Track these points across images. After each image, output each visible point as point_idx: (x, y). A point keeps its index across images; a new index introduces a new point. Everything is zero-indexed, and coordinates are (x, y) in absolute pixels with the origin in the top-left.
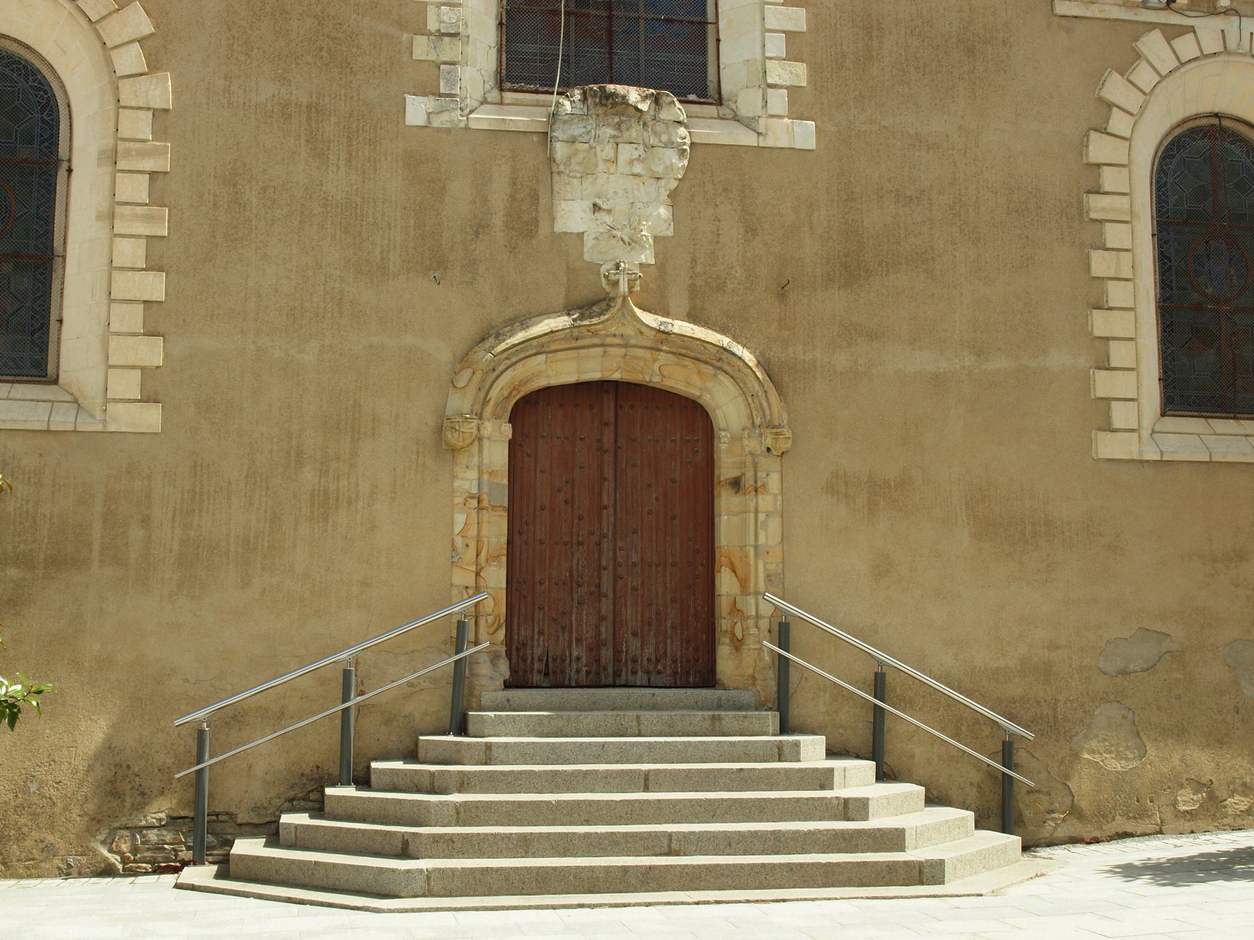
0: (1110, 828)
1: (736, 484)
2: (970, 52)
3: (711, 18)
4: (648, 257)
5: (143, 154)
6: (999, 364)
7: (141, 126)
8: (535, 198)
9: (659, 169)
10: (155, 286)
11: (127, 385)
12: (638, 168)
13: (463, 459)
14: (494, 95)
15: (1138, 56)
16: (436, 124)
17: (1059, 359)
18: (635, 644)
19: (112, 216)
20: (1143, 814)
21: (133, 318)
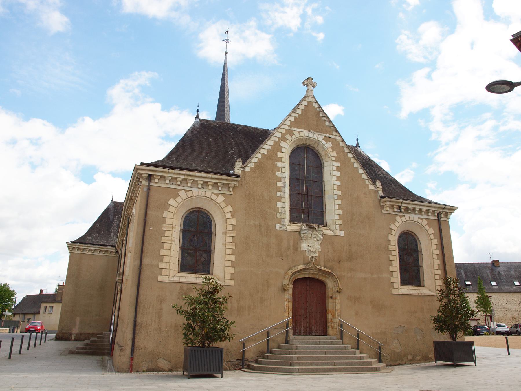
0: (397, 363)
1: (331, 297)
2: (369, 219)
3: (324, 211)
4: (317, 255)
5: (231, 233)
6: (375, 276)
7: (230, 228)
8: (298, 244)
9: (318, 239)
10: (233, 258)
11: (228, 276)
12: (315, 239)
13: (286, 292)
14: (289, 224)
15: (396, 220)
16: (281, 229)
17: (385, 275)
18: (313, 327)
19: (226, 244)
20: (402, 360)
21: (229, 264)
